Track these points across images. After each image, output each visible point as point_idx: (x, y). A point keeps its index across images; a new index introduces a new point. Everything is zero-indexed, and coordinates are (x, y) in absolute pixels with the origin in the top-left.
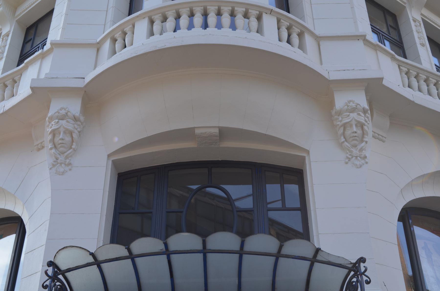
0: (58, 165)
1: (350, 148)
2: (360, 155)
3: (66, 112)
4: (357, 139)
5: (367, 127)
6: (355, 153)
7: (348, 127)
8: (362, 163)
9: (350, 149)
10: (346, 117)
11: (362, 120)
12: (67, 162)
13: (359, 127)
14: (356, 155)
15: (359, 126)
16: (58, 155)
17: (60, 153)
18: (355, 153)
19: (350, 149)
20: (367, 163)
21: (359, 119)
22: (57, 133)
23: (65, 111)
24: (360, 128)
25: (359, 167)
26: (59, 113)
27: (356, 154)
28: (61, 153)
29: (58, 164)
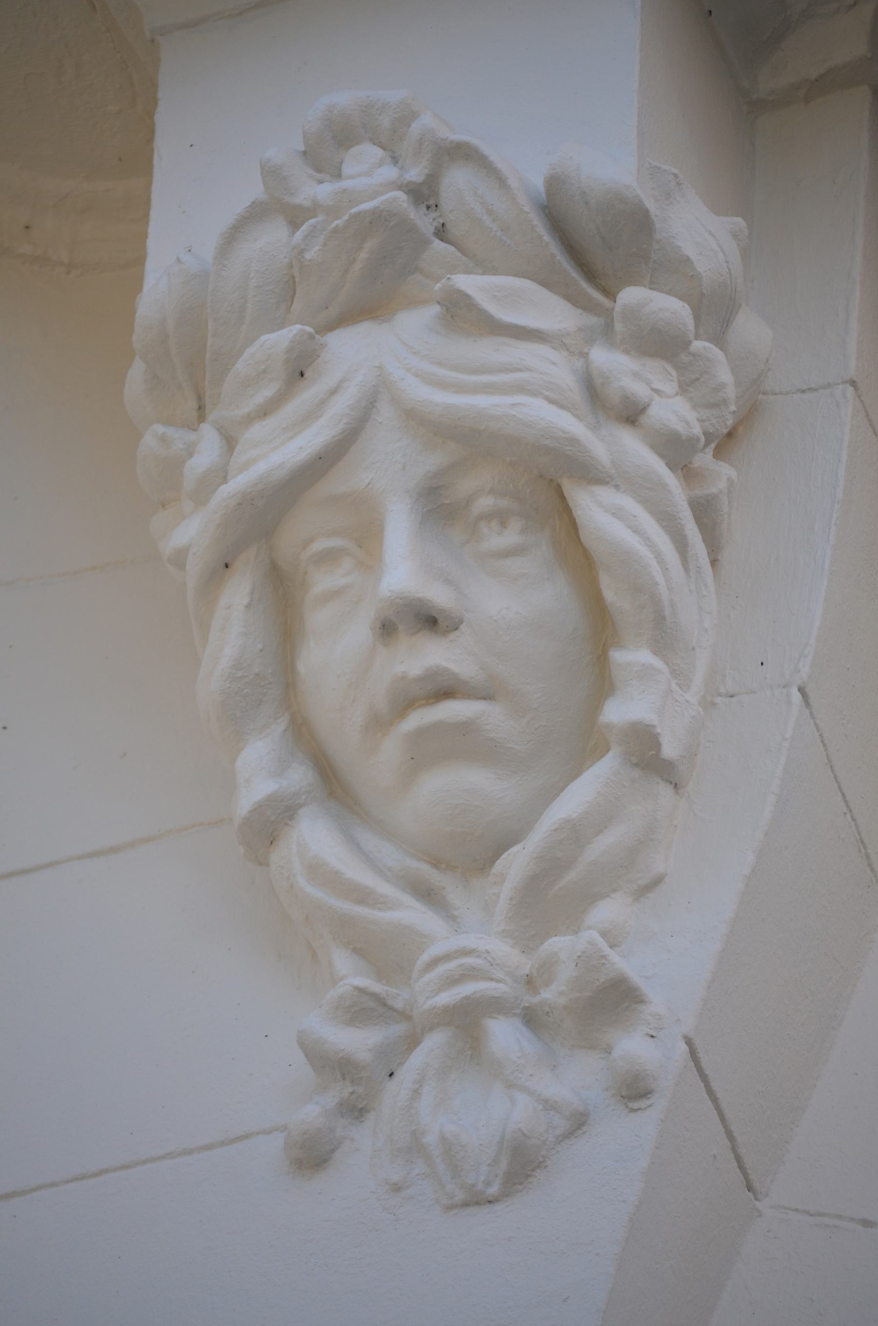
0: (417, 1058)
1: (364, 896)
2: (530, 982)
3: (416, 174)
4: (466, 728)
5: (628, 502)
6: (450, 965)
7: (329, 557)
8: (549, 1105)
9: (378, 915)
10: (265, 411)
11: (520, 388)
12: (566, 972)
13: (501, 518)
14: (447, 998)
15: (485, 503)
16: (408, 900)
17: (425, 869)
18: (447, 957)
19: (378, 915)
20: (645, 1094)
21: (461, 389)
22: (321, 545)
23: (389, 172)
24: (511, 537)
25: (494, 1190)
26: (294, 225)
27: (452, 981)
28: (436, 863)
29: (412, 1042)
